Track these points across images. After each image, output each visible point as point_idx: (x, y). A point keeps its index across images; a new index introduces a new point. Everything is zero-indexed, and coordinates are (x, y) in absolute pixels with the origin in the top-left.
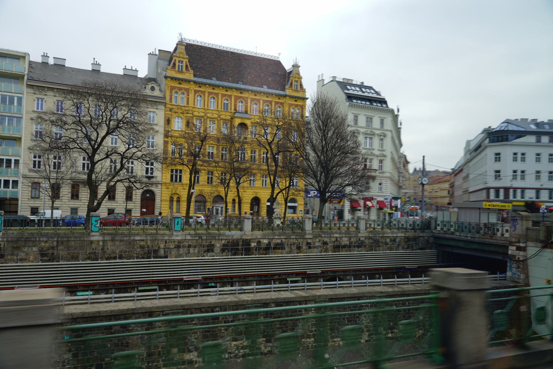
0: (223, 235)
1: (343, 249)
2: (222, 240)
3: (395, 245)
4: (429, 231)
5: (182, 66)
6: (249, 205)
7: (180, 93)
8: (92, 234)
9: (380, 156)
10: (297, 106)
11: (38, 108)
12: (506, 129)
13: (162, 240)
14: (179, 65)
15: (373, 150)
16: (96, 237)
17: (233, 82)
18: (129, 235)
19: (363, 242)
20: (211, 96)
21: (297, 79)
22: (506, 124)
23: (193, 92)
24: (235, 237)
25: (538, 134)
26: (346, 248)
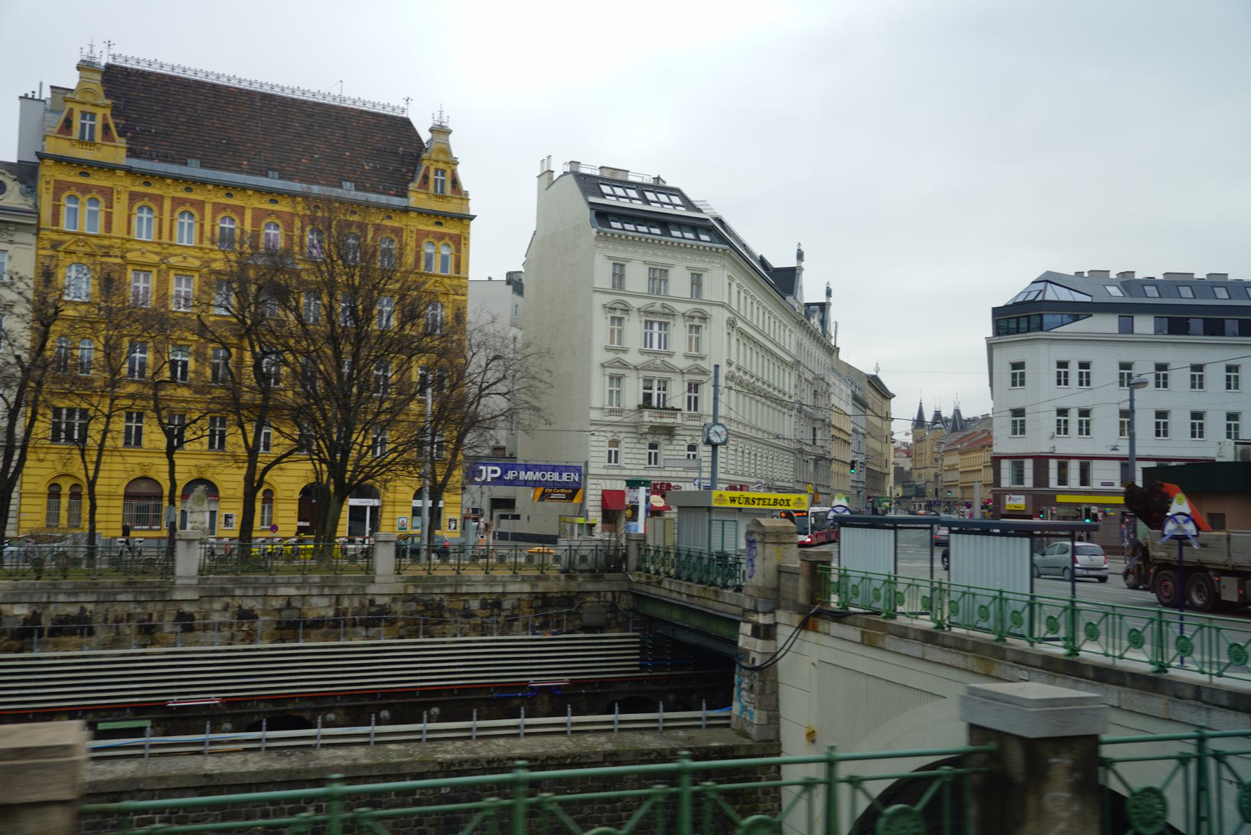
1: (313, 632)
3: (501, 619)
4: (619, 575)
5: (92, 127)
6: (296, 507)
7: (84, 199)
9: (689, 372)
10: (440, 237)
12: (1039, 298)
14: (83, 126)
15: (670, 355)
17: (165, 159)
19: (383, 610)
20: (181, 209)
21: (441, 166)
22: (1041, 286)
25: (1125, 311)
26: (324, 630)
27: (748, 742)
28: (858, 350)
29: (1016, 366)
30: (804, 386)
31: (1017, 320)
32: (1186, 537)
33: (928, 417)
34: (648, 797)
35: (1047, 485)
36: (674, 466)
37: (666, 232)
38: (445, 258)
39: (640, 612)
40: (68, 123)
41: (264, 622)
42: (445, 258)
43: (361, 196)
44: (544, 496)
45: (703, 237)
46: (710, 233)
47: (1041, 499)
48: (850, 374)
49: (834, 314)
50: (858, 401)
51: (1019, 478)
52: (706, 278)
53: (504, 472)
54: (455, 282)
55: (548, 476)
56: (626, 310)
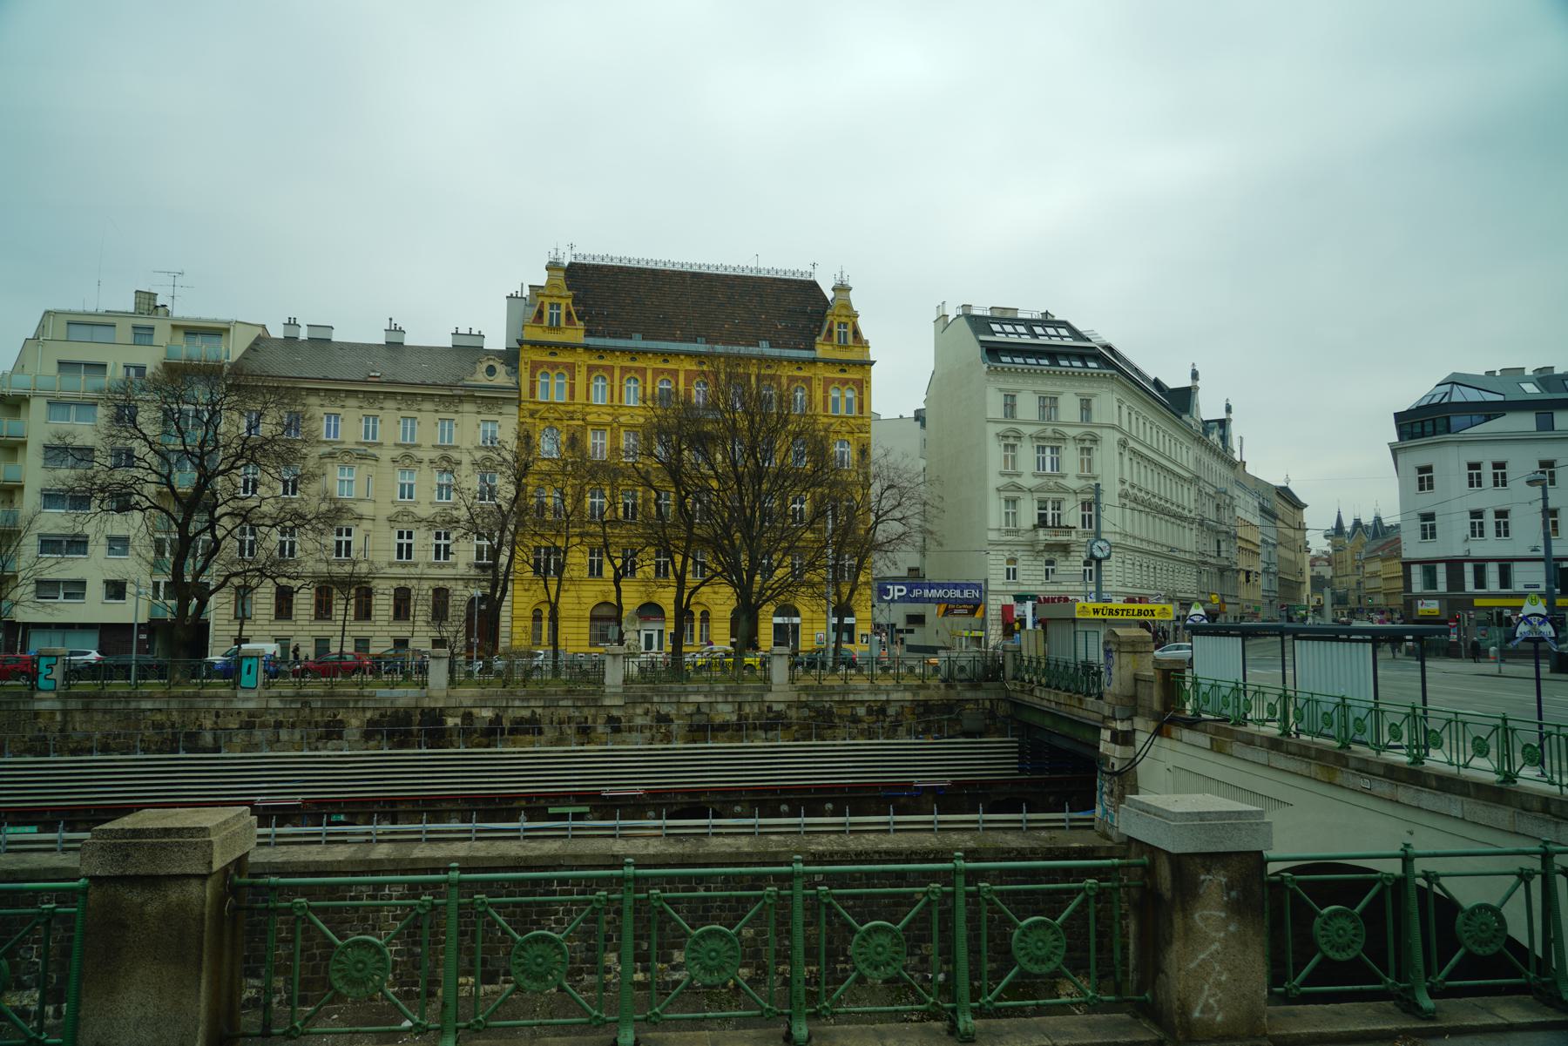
0: (371, 697)
1: (720, 734)
2: (364, 709)
3: (886, 724)
7: (553, 374)
8: (38, 695)
9: (1082, 492)
10: (845, 382)
11: (367, 437)
13: (208, 710)
16: (46, 702)
17: (614, 335)
18: (128, 698)
19: (779, 715)
21: (844, 319)
22: (1447, 388)
23: (584, 370)
24: (400, 703)
27: (1109, 844)
28: (1265, 461)
29: (1422, 470)
30: (1205, 500)
31: (1421, 424)
32: (1542, 640)
33: (1348, 524)
34: (1079, 891)
35: (1463, 589)
36: (1069, 577)
37: (1054, 362)
38: (849, 401)
39: (1016, 719)
40: (540, 313)
41: (678, 725)
42: (849, 401)
43: (776, 352)
44: (948, 612)
45: (1091, 364)
46: (1101, 361)
47: (1457, 603)
48: (1258, 488)
49: (1235, 431)
50: (1267, 513)
51: (1431, 581)
52: (1095, 403)
53: (910, 591)
55: (950, 593)
56: (1019, 438)
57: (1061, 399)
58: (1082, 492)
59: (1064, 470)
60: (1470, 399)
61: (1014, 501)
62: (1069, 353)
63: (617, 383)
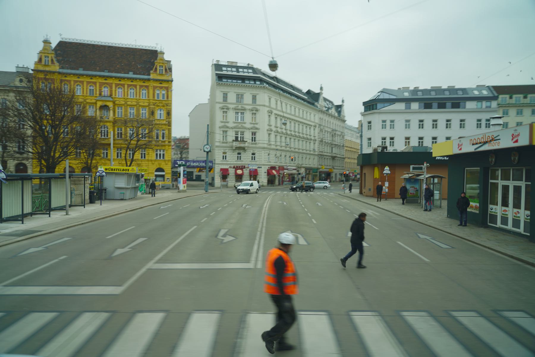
15: (245, 123)
38: (163, 95)
42: (163, 95)
52: (257, 97)
54: (167, 102)
56: (228, 109)
57: (245, 95)
58: (252, 129)
59: (245, 121)
60: (385, 98)
61: (226, 132)
62: (249, 78)
63: (126, 90)
